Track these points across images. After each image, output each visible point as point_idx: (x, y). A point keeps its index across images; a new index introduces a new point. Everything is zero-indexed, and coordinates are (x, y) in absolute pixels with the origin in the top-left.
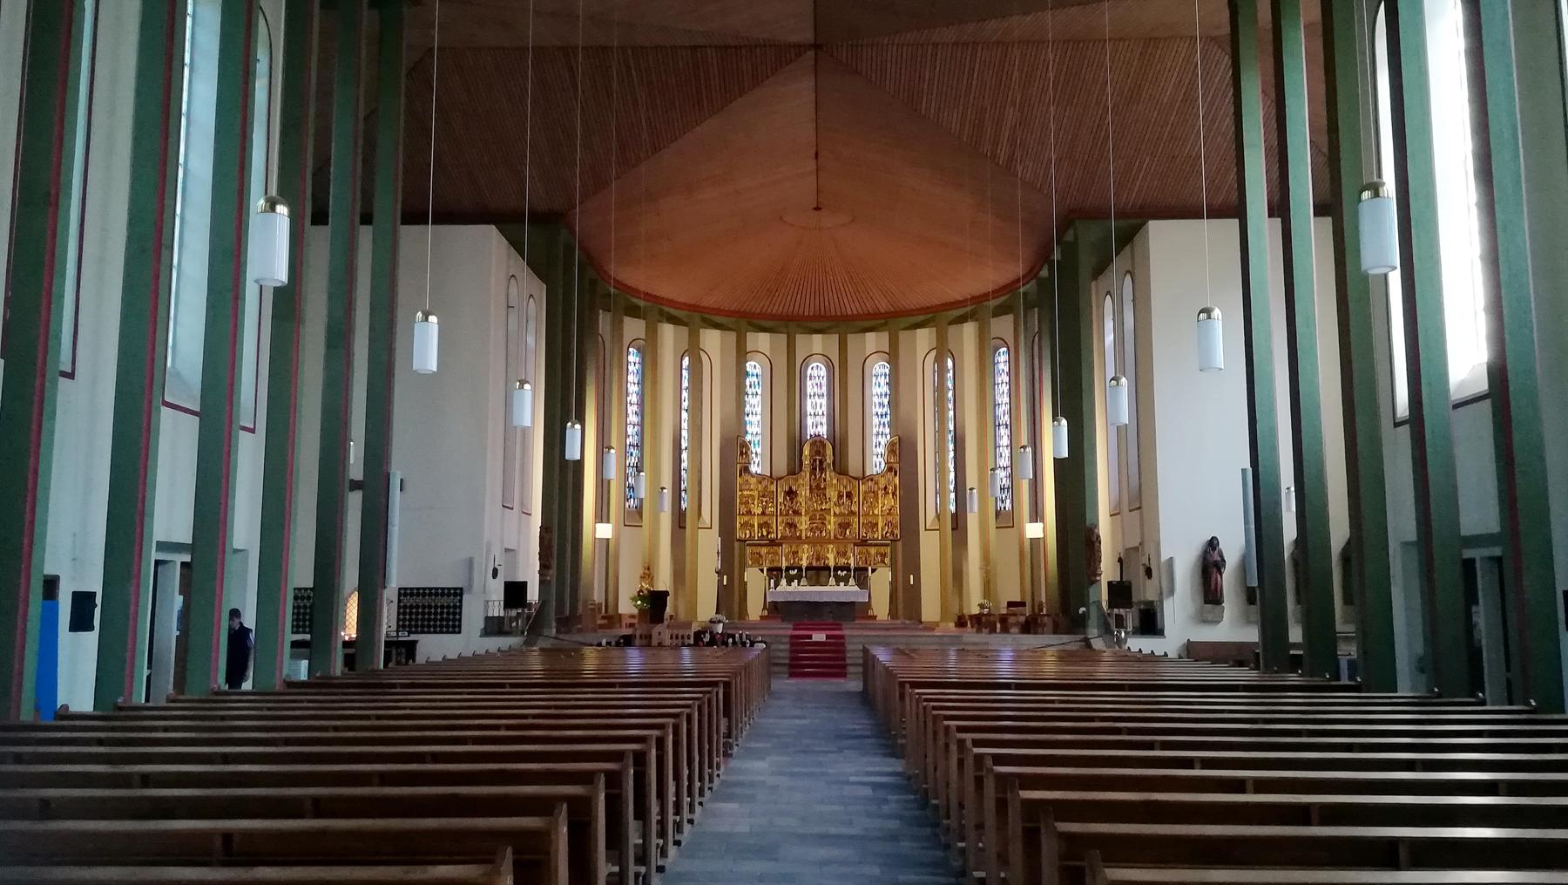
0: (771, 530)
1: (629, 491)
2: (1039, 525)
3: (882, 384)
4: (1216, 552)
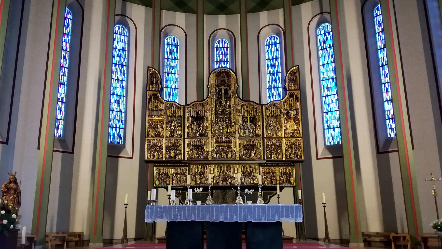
0: (179, 152)
3: (273, 50)
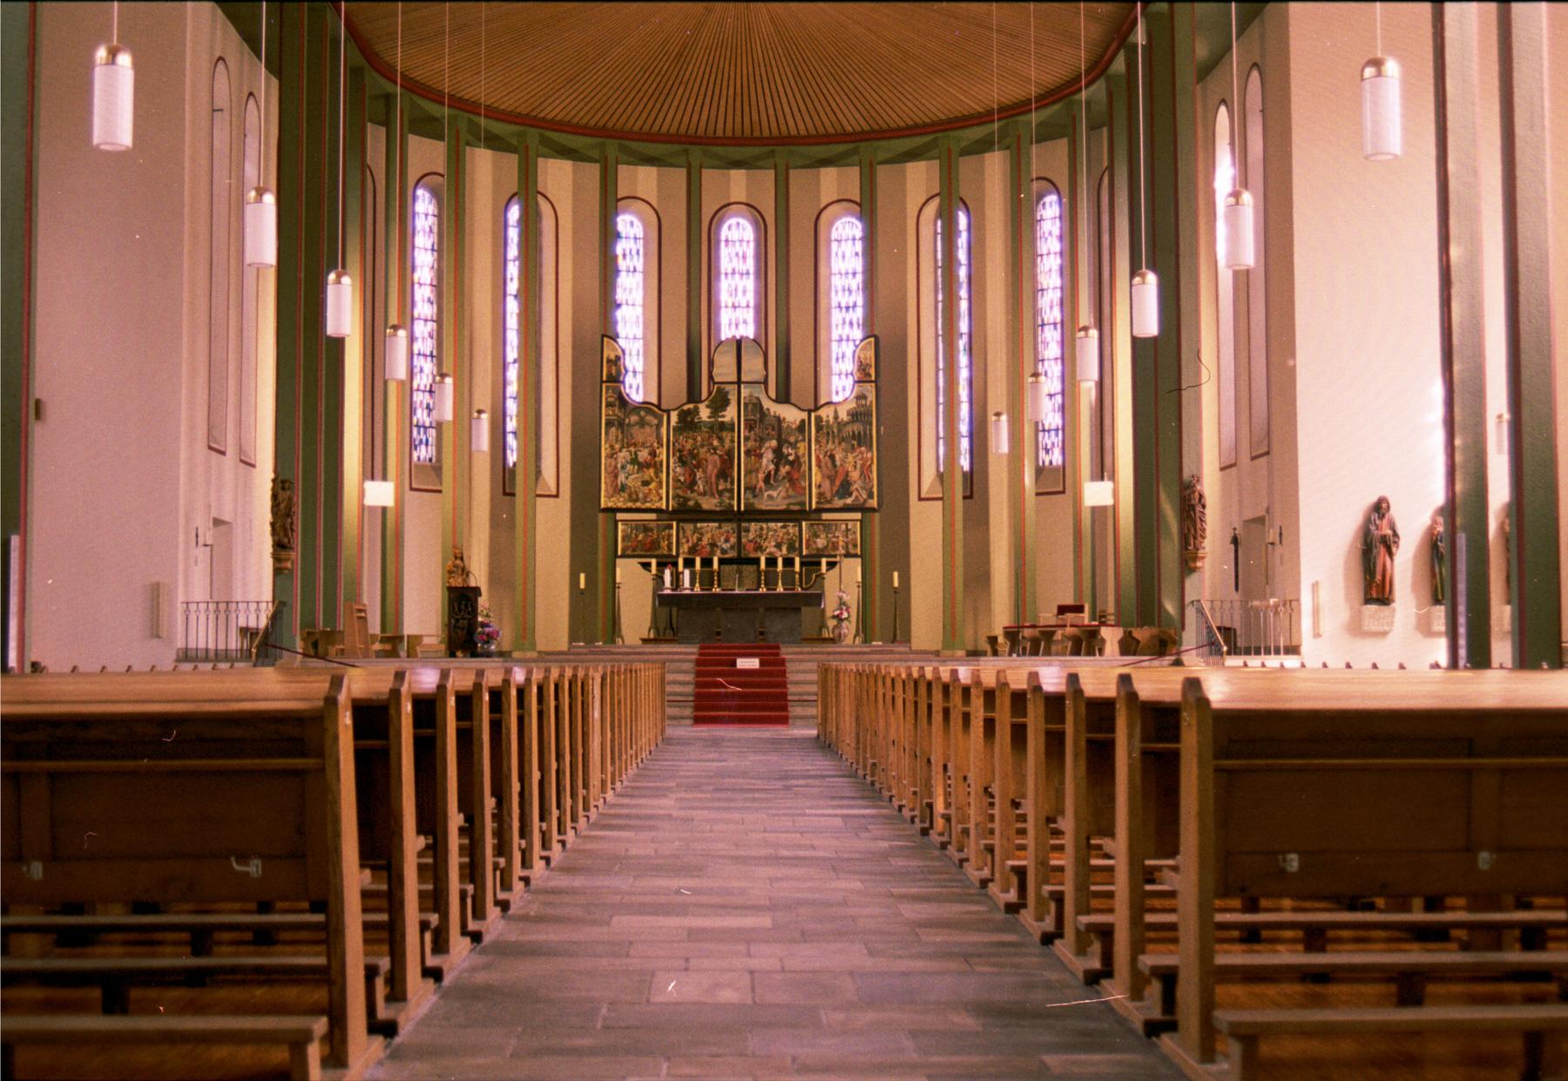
1: (419, 433)
2: (1107, 485)
3: (848, 254)
4: (1385, 521)
